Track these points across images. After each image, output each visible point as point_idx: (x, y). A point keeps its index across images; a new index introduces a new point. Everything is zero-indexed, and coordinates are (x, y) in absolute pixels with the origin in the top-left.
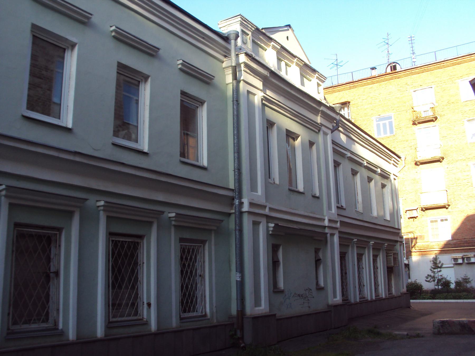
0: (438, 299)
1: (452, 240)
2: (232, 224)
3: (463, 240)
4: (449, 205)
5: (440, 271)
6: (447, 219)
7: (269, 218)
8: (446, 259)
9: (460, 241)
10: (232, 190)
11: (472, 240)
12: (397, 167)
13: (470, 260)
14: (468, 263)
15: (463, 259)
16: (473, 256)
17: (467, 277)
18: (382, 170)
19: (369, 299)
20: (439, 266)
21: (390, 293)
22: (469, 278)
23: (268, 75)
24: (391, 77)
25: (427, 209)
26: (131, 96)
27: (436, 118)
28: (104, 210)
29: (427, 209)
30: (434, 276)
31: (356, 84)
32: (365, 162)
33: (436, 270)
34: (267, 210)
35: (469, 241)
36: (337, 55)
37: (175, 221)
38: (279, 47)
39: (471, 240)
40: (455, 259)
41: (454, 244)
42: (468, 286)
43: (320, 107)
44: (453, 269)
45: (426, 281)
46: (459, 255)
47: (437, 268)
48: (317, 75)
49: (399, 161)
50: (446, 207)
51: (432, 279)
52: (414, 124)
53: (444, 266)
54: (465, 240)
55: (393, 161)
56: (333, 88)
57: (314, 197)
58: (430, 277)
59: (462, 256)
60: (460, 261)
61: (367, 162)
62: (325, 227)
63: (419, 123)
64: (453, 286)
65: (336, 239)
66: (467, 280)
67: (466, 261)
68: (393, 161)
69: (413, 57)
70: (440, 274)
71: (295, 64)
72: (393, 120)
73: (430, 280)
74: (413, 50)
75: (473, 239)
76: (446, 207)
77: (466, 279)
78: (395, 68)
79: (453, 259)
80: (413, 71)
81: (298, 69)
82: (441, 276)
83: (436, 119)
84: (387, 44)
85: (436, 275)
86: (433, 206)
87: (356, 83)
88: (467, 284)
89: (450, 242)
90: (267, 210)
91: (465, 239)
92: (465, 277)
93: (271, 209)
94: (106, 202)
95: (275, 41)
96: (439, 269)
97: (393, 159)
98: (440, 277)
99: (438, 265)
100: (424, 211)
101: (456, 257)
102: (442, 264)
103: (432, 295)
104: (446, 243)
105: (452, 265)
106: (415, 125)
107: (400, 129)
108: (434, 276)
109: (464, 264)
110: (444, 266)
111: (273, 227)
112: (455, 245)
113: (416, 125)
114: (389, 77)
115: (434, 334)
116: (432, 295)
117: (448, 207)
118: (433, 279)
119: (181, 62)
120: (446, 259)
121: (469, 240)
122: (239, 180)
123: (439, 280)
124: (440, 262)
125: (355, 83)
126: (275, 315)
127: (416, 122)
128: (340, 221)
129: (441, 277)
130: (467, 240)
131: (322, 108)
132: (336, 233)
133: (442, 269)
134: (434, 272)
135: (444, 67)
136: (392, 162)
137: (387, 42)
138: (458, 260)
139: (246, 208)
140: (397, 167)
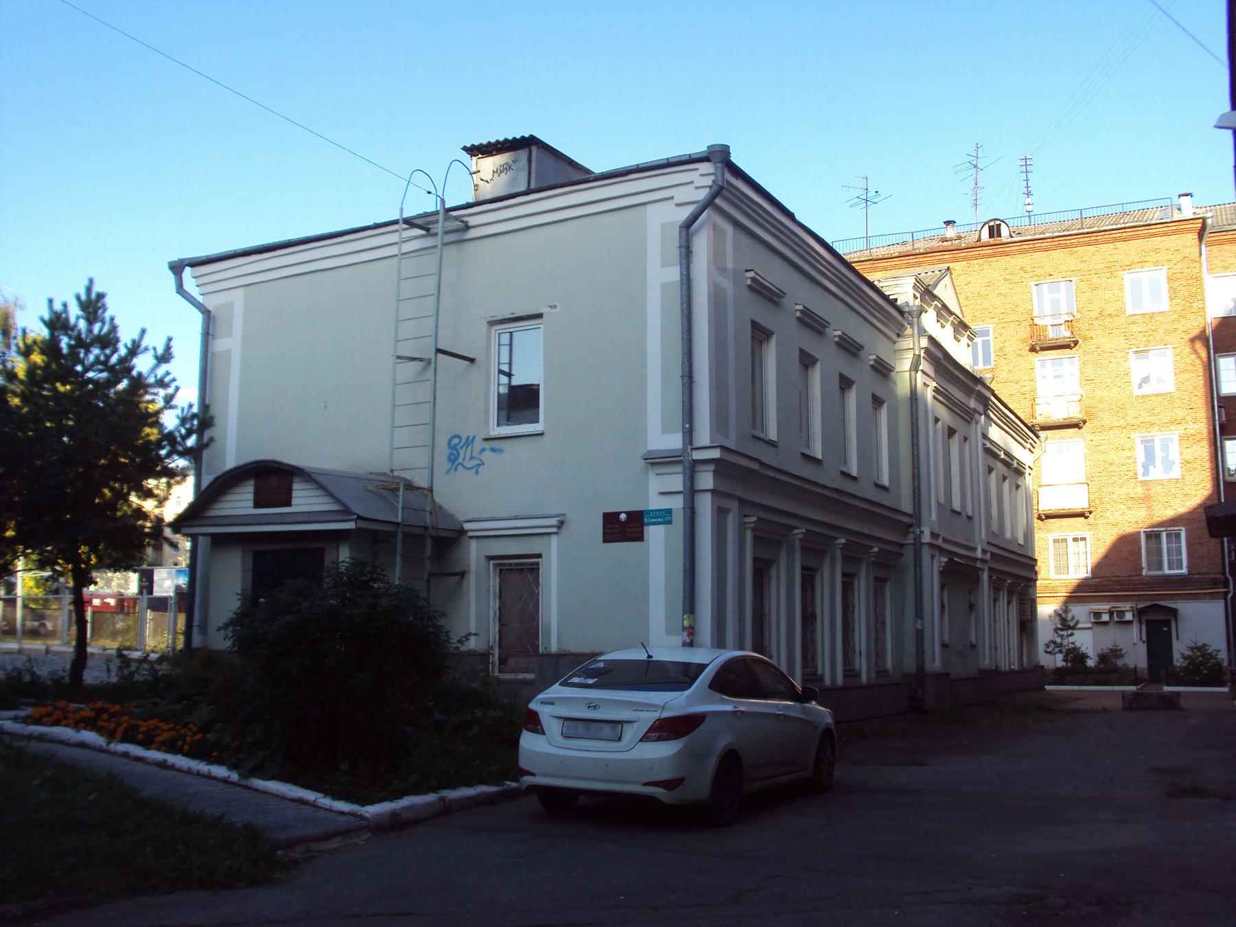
0: (1068, 685)
1: (1092, 578)
2: (908, 559)
3: (1113, 579)
4: (1090, 512)
5: (1072, 635)
6: (1085, 538)
7: (943, 551)
8: (1080, 612)
9: (1107, 580)
10: (911, 516)
11: (1129, 580)
12: (1032, 453)
13: (1100, 617)
14: (1118, 623)
15: (1111, 613)
16: (1130, 609)
17: (1118, 646)
18: (1007, 454)
19: (1003, 669)
20: (1072, 625)
21: (1022, 665)
22: (1121, 650)
23: (942, 357)
24: (991, 251)
25: (1048, 517)
26: (1153, 540)
27: (1076, 343)
28: (841, 549)
29: (1048, 517)
30: (1061, 644)
31: (921, 260)
32: (1002, 453)
33: (1065, 633)
34: (940, 540)
35: (1122, 580)
36: (867, 178)
37: (875, 557)
38: (940, 306)
39: (1126, 578)
40: (1097, 614)
41: (1095, 586)
42: (1120, 663)
43: (976, 385)
44: (1090, 631)
45: (1046, 652)
46: (1103, 607)
47: (1067, 630)
48: (968, 333)
49: (1036, 443)
50: (1086, 515)
51: (1057, 650)
52: (1033, 349)
53: (1079, 626)
54: (1116, 579)
55: (1030, 443)
56: (872, 262)
57: (953, 511)
58: (1053, 646)
59: (1109, 609)
60: (1105, 618)
61: (1004, 454)
62: (976, 559)
63: (1043, 349)
64: (1090, 663)
65: (985, 576)
66: (1118, 653)
67: (1116, 619)
68: (1030, 443)
69: (1028, 200)
70: (1071, 639)
71: (950, 323)
72: (991, 338)
73: (1054, 650)
74: (1029, 185)
75: (1130, 578)
76: (1084, 514)
77: (1116, 651)
78: (994, 231)
79: (1092, 614)
80: (1036, 245)
81: (952, 329)
82: (1073, 643)
83: (1076, 345)
84: (976, 166)
85: (1065, 642)
86: (1062, 511)
87: (922, 256)
88: (1118, 661)
89: (1088, 581)
90: (940, 540)
91: (1116, 576)
92: (1114, 646)
93: (945, 540)
94: (847, 540)
95: (940, 299)
96: (1069, 632)
97: (1031, 441)
98: (1071, 646)
99: (1069, 623)
100: (1042, 520)
101: (1098, 609)
102: (1077, 623)
103: (1057, 677)
104: (1082, 582)
105: (1090, 625)
106: (1034, 353)
107: (1005, 357)
108: (1061, 644)
109: (1111, 623)
110: (1079, 626)
111: (946, 563)
112: (1097, 588)
113: (1037, 352)
114: (988, 252)
115: (1124, 709)
116: (1057, 677)
117: (1088, 514)
118: (1059, 649)
119: (874, 357)
120: (1080, 612)
121: (1123, 578)
122: (917, 502)
123: (1069, 651)
124: (1073, 618)
125: (918, 256)
126: (948, 675)
127: (1038, 348)
128: (991, 552)
129: (1073, 646)
130: (1120, 579)
131: (979, 388)
132: (986, 567)
133: (1076, 632)
134: (1062, 636)
135: (1096, 243)
136: (1028, 446)
137: (974, 163)
138: (1124, 615)
139: (926, 538)
140: (1032, 453)
